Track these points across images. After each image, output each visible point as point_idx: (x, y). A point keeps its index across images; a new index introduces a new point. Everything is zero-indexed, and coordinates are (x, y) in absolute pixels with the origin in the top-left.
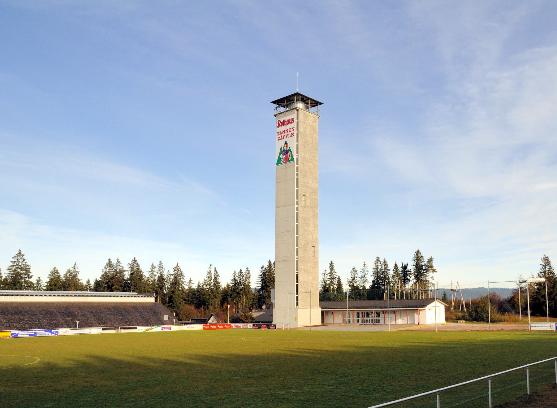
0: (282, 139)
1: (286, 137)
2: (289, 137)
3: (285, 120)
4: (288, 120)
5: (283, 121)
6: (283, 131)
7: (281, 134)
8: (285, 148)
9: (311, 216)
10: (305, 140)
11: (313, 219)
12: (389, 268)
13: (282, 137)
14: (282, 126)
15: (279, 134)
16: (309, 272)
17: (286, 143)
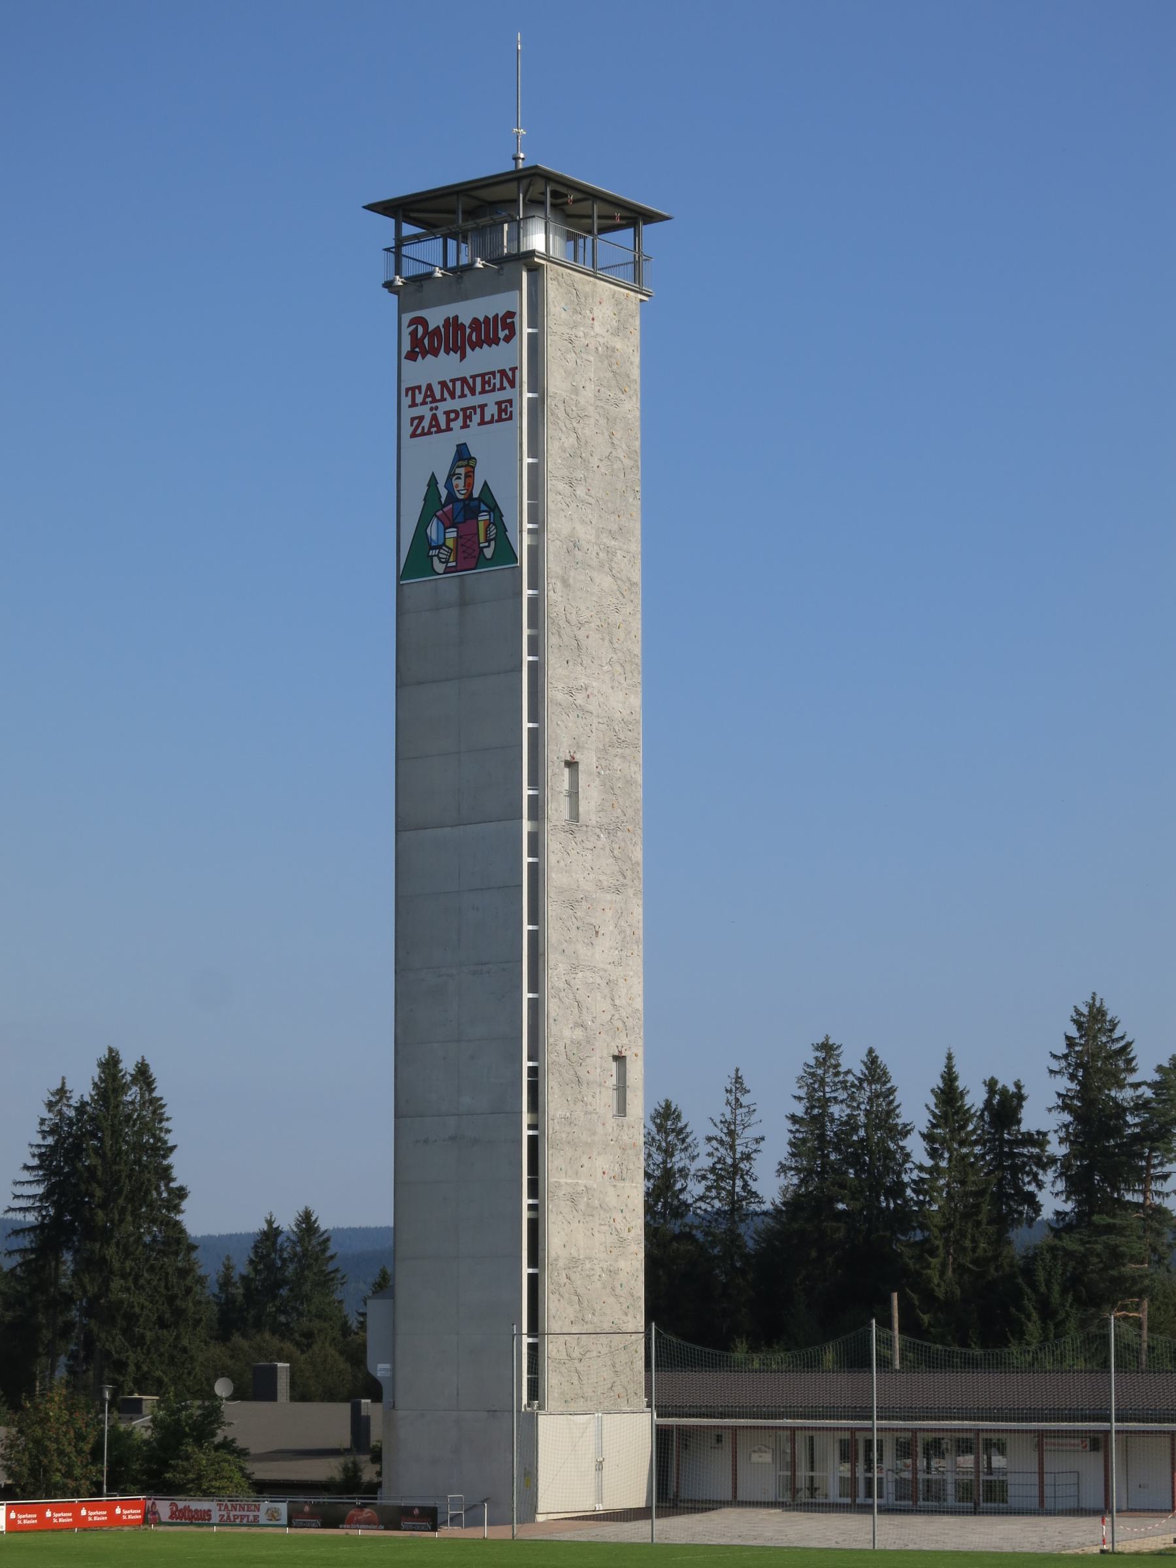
0: (439, 431)
1: (460, 421)
2: (482, 422)
3: (456, 318)
4: (475, 320)
5: (441, 323)
6: (443, 384)
7: (434, 400)
8: (459, 484)
9: (605, 884)
10: (572, 440)
11: (615, 897)
12: (905, 1116)
13: (434, 417)
14: (435, 353)
15: (419, 398)
16: (597, 1203)
17: (463, 455)
